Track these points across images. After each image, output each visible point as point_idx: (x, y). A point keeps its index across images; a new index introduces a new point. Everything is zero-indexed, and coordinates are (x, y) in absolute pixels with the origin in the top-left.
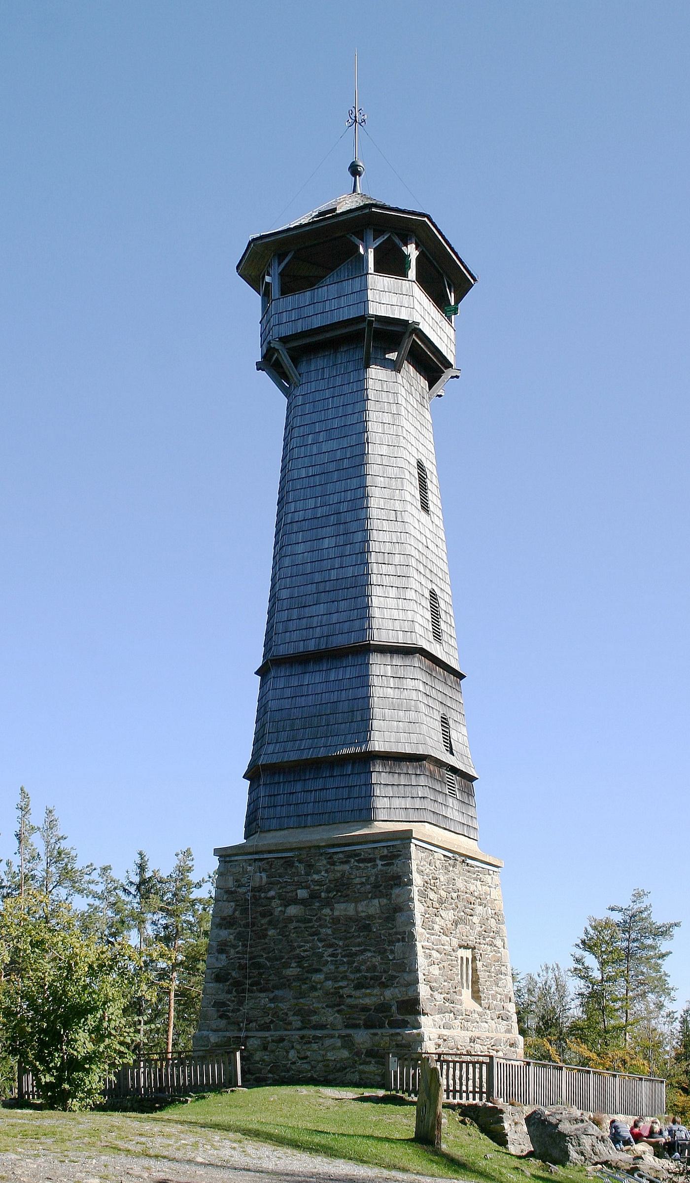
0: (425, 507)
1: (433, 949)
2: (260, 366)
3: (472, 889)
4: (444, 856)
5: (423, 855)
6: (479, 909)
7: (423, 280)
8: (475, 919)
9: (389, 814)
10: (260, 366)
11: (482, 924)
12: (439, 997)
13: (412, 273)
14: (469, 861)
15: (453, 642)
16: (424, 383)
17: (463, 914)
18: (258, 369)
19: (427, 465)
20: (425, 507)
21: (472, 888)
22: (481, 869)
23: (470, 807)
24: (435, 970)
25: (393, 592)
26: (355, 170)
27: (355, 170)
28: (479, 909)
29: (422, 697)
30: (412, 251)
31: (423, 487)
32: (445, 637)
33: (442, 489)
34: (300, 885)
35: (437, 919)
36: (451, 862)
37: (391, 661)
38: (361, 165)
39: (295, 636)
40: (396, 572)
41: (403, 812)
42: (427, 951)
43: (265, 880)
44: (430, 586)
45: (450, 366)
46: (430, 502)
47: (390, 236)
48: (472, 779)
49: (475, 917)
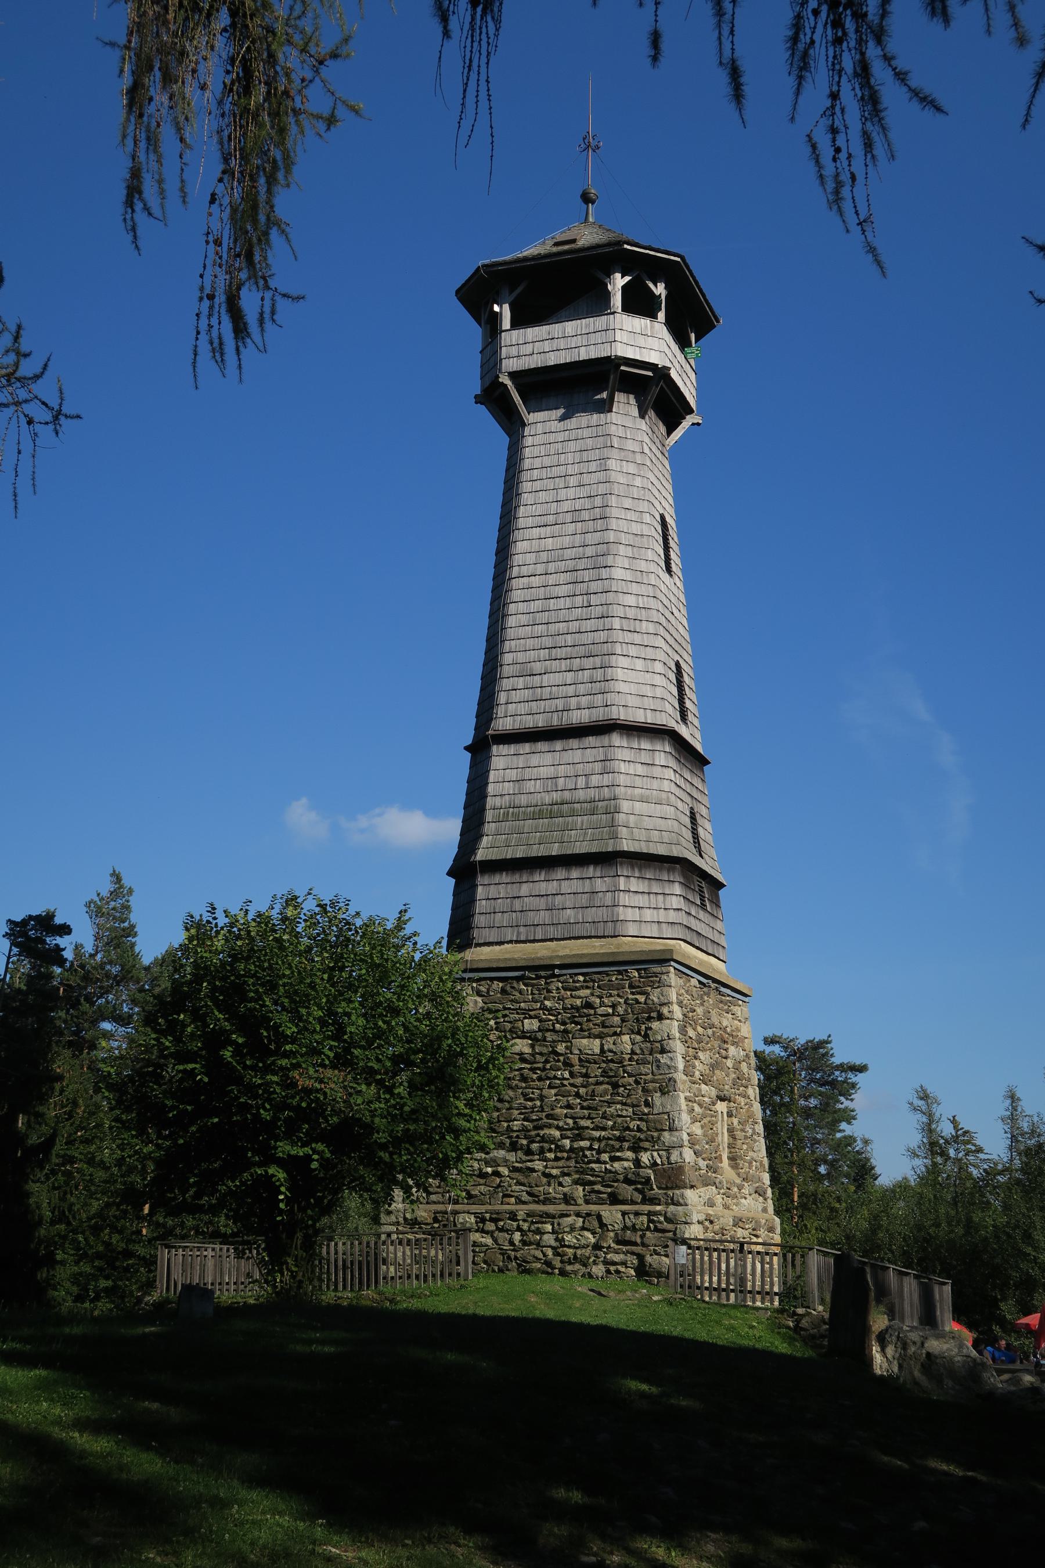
0: (669, 570)
1: (695, 1102)
2: (478, 400)
3: (724, 1024)
4: (700, 982)
5: (681, 981)
6: (732, 1051)
7: (669, 323)
8: (729, 1063)
9: (660, 930)
10: (478, 400)
11: (737, 1068)
12: (703, 1164)
13: (661, 315)
14: (722, 989)
15: (696, 722)
16: (663, 429)
17: (717, 1056)
18: (476, 403)
19: (668, 519)
20: (669, 570)
21: (725, 1023)
22: (731, 999)
23: (718, 921)
24: (697, 1129)
25: (639, 664)
26: (586, 198)
27: (586, 198)
28: (732, 1051)
29: (674, 789)
30: (660, 289)
31: (667, 548)
32: (690, 717)
33: (680, 545)
34: (527, 1014)
35: (697, 1063)
36: (706, 989)
37: (639, 743)
38: (593, 191)
39: (523, 708)
40: (643, 641)
41: (655, 926)
42: (690, 1104)
43: (481, 1004)
44: (677, 658)
45: (691, 411)
46: (672, 562)
47: (638, 275)
48: (720, 885)
49: (729, 1060)
